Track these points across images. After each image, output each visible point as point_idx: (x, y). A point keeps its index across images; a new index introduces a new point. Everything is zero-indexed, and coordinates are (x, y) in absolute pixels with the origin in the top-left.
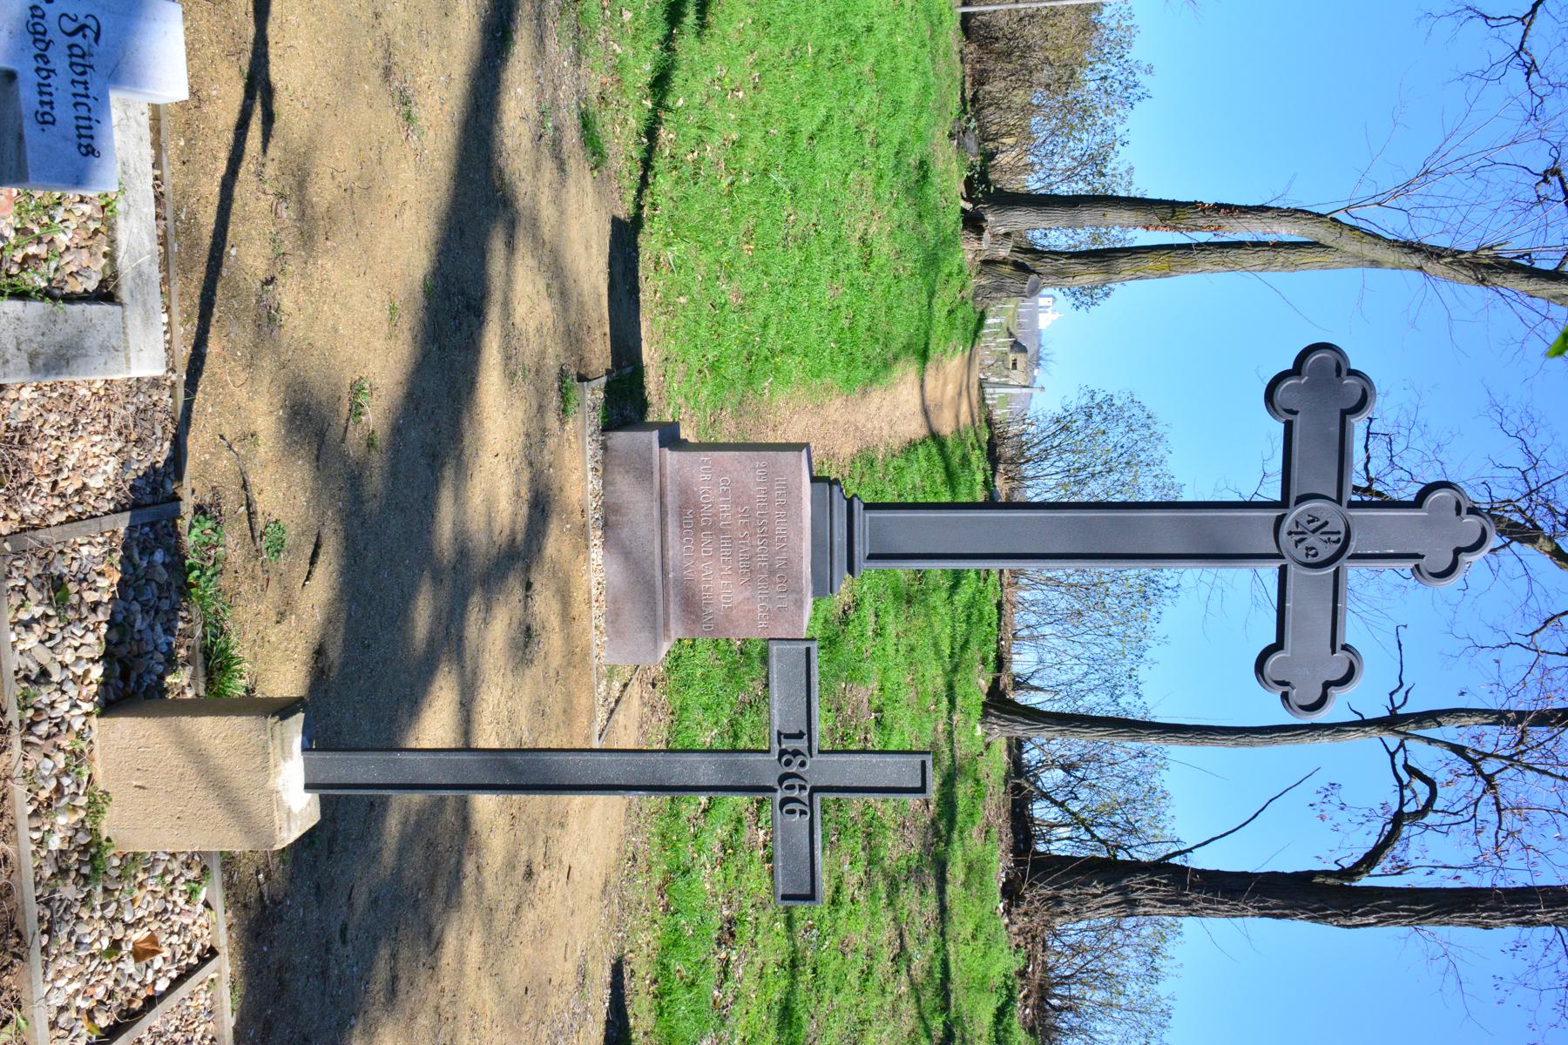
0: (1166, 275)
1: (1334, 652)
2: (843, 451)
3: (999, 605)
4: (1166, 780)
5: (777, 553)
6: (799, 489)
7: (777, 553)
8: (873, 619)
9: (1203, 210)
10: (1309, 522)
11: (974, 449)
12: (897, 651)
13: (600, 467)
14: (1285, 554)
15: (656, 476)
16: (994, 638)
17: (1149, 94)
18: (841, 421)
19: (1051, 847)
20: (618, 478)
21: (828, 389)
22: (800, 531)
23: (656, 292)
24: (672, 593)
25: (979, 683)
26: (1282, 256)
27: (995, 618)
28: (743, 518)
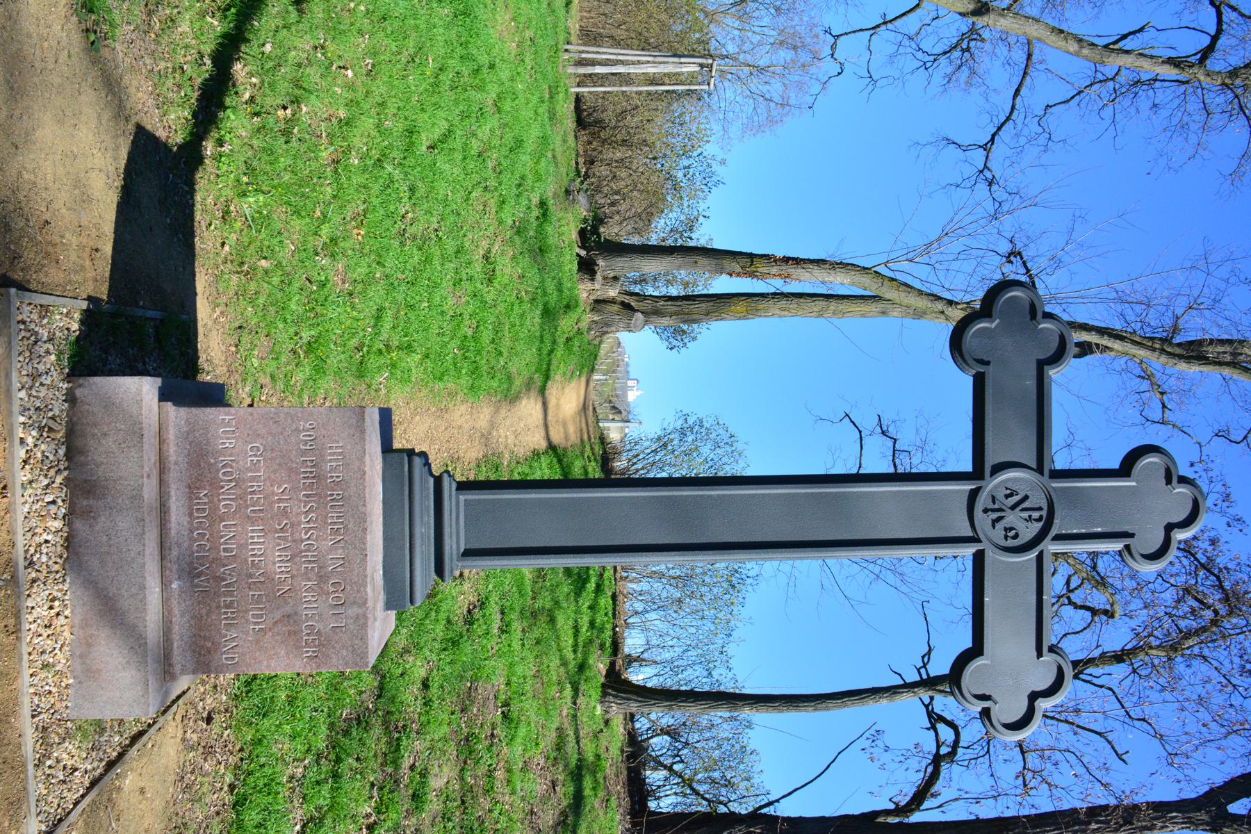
0: (745, 318)
1: (1040, 655)
2: (468, 455)
3: (614, 597)
4: (753, 739)
8: (499, 616)
9: (775, 261)
10: (1007, 496)
11: (590, 461)
12: (523, 645)
14: (982, 537)
16: (609, 626)
17: (724, 181)
18: (466, 427)
19: (662, 804)
21: (452, 395)
23: (223, 244)
24: (176, 611)
25: (600, 666)
26: (833, 305)
27: (610, 608)
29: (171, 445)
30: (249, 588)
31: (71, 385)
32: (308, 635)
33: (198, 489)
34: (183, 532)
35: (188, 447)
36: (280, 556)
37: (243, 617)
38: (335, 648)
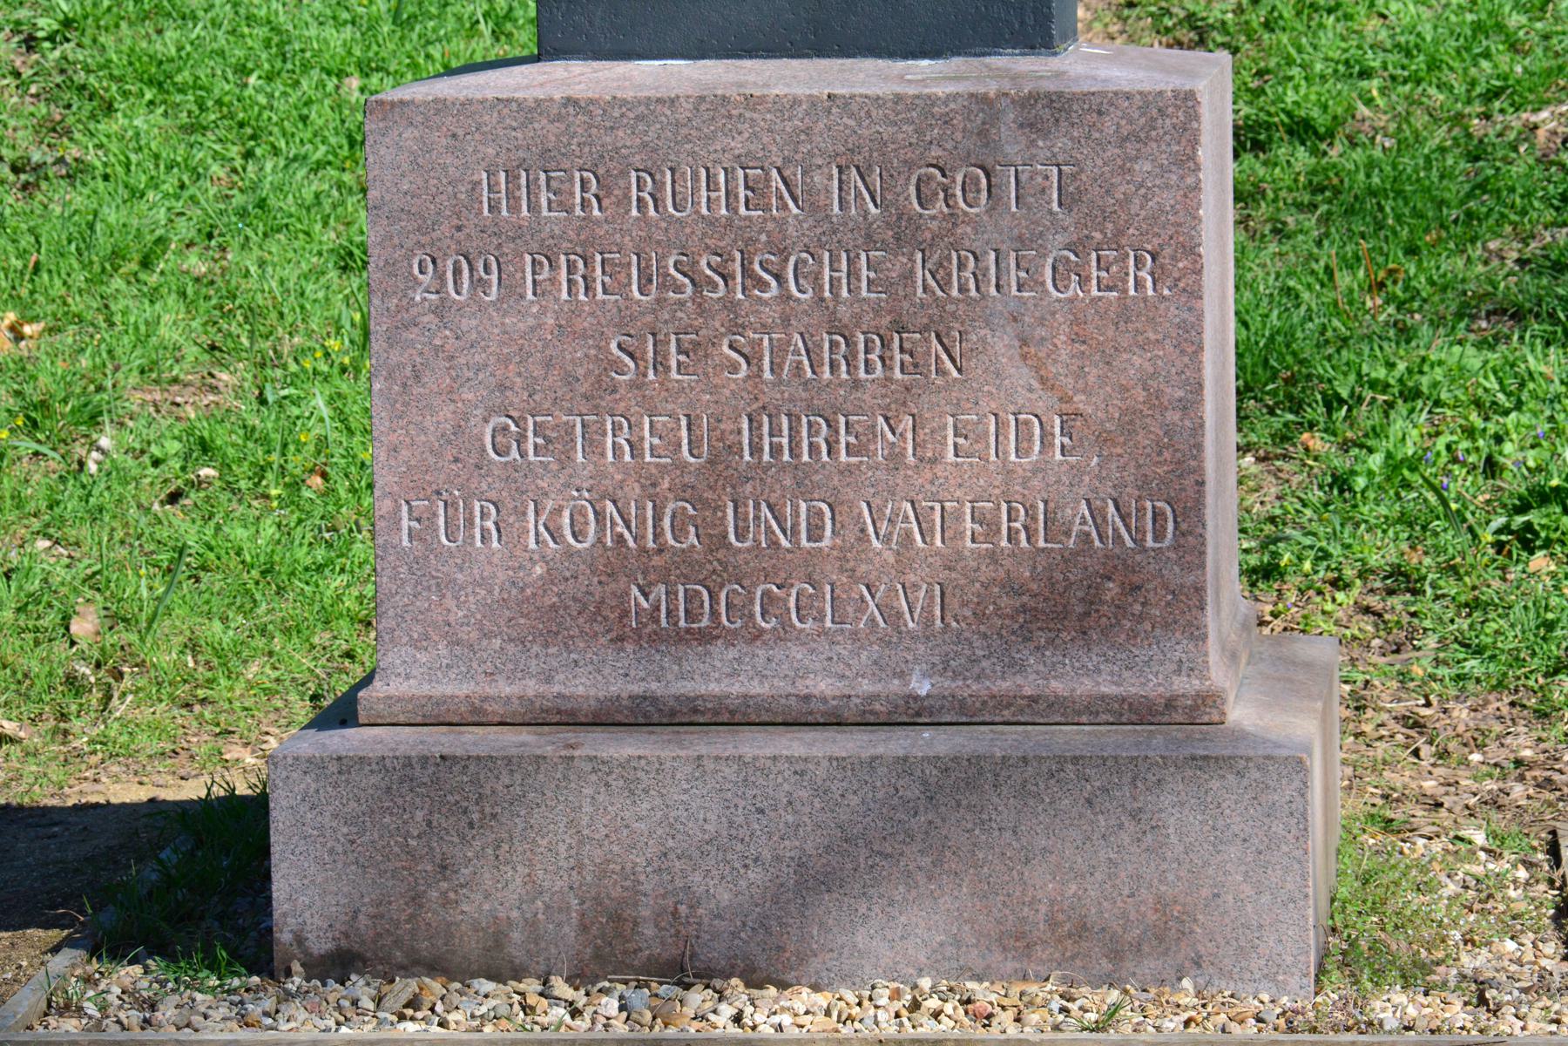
5: (814, 207)
6: (530, 111)
7: (814, 207)
13: (405, 988)
15: (440, 741)
20: (473, 908)
22: (714, 106)
24: (1004, 686)
28: (660, 364)
29: (491, 691)
30: (934, 461)
31: (296, 967)
32: (1084, 281)
33: (625, 614)
34: (760, 661)
35: (497, 643)
36: (834, 366)
37: (1025, 482)
38: (1127, 199)
